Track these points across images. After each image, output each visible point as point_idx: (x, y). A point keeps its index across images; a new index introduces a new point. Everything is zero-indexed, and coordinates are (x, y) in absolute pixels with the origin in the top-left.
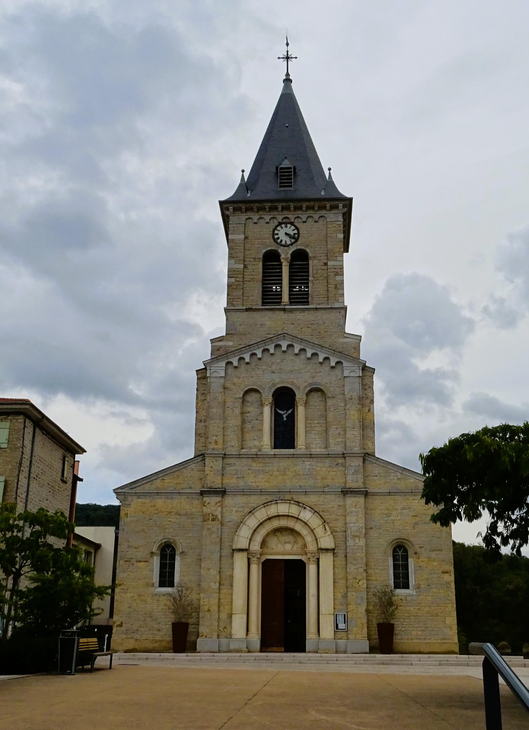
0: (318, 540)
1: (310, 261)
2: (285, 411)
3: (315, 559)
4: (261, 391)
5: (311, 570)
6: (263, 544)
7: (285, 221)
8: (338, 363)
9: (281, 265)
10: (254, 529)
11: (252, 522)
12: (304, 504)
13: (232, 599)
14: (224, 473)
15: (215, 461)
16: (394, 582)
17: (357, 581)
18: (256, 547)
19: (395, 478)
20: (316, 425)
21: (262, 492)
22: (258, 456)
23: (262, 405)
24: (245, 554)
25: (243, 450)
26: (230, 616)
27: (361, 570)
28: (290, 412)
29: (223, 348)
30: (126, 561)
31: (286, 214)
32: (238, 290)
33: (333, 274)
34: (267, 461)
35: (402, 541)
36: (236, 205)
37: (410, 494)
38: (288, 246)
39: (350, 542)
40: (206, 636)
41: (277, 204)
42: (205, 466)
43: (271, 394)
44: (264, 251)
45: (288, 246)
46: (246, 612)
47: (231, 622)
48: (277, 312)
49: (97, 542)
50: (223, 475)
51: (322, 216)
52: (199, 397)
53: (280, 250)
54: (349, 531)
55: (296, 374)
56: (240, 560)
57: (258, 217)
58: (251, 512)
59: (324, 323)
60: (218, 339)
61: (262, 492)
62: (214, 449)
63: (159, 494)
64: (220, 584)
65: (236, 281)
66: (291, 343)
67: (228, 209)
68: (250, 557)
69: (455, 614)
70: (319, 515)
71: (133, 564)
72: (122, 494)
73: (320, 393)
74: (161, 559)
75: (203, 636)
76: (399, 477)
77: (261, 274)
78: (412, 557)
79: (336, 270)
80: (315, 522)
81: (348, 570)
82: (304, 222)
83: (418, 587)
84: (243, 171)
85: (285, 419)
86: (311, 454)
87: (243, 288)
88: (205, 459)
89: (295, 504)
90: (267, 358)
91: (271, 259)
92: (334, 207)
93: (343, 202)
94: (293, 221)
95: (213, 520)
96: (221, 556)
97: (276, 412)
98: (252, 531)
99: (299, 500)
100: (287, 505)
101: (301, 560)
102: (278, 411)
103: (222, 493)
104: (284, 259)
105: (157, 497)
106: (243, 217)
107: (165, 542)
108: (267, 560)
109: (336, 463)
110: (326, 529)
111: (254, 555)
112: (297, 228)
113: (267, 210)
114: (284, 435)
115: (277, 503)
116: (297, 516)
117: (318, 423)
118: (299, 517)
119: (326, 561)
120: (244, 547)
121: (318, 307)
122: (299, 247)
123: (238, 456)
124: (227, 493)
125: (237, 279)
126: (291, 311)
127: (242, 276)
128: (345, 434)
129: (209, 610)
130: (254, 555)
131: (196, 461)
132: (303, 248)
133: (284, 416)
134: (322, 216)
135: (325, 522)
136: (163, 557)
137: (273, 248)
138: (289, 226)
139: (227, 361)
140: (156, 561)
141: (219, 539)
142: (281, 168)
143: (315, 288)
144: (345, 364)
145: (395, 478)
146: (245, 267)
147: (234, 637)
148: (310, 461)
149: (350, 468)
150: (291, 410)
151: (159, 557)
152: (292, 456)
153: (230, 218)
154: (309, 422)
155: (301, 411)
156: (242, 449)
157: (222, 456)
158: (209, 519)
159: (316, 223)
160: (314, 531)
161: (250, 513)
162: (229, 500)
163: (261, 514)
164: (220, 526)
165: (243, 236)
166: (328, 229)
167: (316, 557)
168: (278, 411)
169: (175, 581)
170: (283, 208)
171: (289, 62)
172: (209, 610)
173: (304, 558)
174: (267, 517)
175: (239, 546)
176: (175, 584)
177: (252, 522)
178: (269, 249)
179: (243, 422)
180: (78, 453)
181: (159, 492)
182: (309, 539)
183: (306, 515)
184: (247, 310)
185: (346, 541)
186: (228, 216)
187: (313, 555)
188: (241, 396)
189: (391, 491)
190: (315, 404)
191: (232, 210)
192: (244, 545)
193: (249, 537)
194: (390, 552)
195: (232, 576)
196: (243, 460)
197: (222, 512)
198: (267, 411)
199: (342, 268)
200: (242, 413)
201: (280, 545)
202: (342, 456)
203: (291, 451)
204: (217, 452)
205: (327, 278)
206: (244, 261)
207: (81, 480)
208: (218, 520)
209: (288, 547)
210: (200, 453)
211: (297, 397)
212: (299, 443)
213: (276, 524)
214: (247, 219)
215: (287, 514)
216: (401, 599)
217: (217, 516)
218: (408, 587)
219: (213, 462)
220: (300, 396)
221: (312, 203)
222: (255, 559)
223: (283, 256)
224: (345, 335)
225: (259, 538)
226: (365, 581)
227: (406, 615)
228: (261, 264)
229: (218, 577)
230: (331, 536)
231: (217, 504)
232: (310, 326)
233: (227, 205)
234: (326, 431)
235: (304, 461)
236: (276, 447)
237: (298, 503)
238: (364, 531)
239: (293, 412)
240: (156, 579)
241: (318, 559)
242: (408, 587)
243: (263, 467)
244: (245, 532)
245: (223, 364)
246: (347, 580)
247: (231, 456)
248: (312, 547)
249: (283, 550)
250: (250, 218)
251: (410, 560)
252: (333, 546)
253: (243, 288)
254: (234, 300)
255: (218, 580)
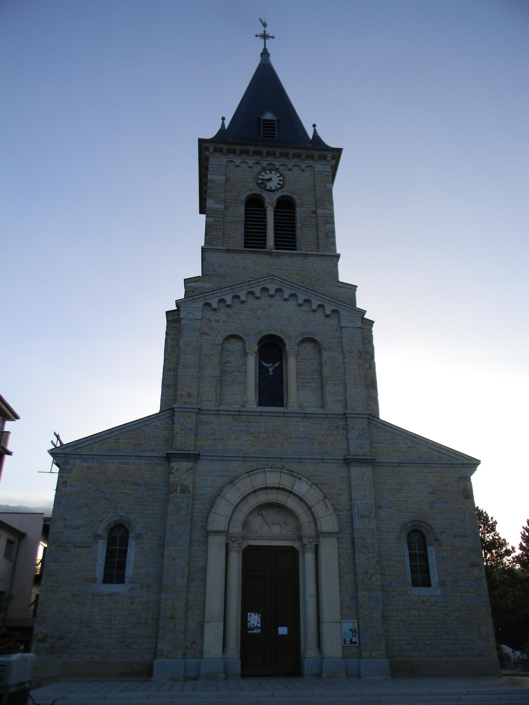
0: (318, 520)
1: (298, 209)
2: (271, 364)
3: (312, 546)
4: (245, 338)
5: (308, 560)
6: (245, 524)
7: (269, 167)
8: (335, 311)
9: (265, 211)
10: (235, 504)
11: (233, 495)
12: (298, 474)
13: (205, 601)
14: (197, 432)
15: (187, 417)
16: (412, 579)
17: (369, 576)
18: (236, 529)
19: (406, 446)
20: (310, 381)
21: (245, 459)
22: (241, 413)
23: (245, 353)
24: (222, 539)
25: (222, 406)
26: (201, 625)
27: (373, 561)
28: (277, 365)
29: (199, 290)
30: (59, 546)
31: (270, 159)
32: (218, 230)
33: (322, 222)
34: (251, 420)
35: (419, 523)
36: (217, 146)
37: (424, 465)
38: (273, 191)
39: (358, 525)
40: (167, 656)
41: (262, 149)
42: (173, 423)
43: (256, 342)
44: (247, 194)
45: (273, 191)
46: (222, 619)
47: (202, 633)
48: (263, 256)
49: (23, 530)
50: (196, 434)
51: (309, 166)
52: (169, 342)
53: (265, 195)
54: (356, 510)
55: (286, 319)
56: (216, 545)
57: (240, 161)
58: (232, 482)
59: (315, 270)
60: (193, 280)
61: (245, 459)
62: (186, 403)
63: (112, 457)
64: (189, 580)
65: (215, 221)
66: (280, 287)
67: (207, 149)
68: (229, 542)
69: (490, 621)
70: (318, 487)
71: (69, 551)
72: (63, 455)
73: (312, 345)
74: (109, 544)
75: (162, 655)
76: (409, 445)
77: (243, 216)
78: (432, 545)
79: (326, 219)
80: (312, 496)
81: (357, 560)
82: (290, 170)
83: (442, 584)
84: (223, 119)
85: (271, 373)
86: (306, 414)
87: (223, 229)
88: (174, 415)
89: (287, 473)
90: (252, 302)
91: (254, 204)
92: (323, 158)
93: (332, 153)
94: (278, 167)
95: (182, 491)
96: (191, 541)
97: (260, 364)
98: (233, 507)
99: (292, 469)
100: (278, 474)
101: (293, 547)
102: (263, 363)
103: (196, 457)
104: (269, 203)
105: (110, 461)
106: (224, 160)
107: (115, 521)
108: (249, 547)
109: (335, 425)
110: (327, 506)
111: (234, 539)
112: (281, 175)
113: (251, 153)
114: (271, 391)
115: (265, 472)
116: (290, 489)
117: (312, 379)
118: (293, 490)
119: (329, 550)
120: (222, 529)
121: (308, 253)
122: (285, 194)
123: (216, 412)
124: (201, 458)
125: (217, 219)
126: (278, 256)
127: (222, 216)
128: (346, 391)
129: (172, 617)
130: (234, 539)
131: (161, 418)
132: (290, 194)
133: (270, 370)
134: (309, 166)
135: (325, 497)
136: (111, 541)
137: (257, 192)
138: (274, 172)
139: (205, 302)
140: (102, 547)
141: (190, 517)
142: (264, 120)
143: (304, 234)
144: (342, 312)
145: (406, 446)
146: (226, 208)
147: (206, 656)
148: (304, 422)
149: (353, 431)
150: (279, 363)
151: (106, 541)
152: (282, 415)
153: (210, 159)
154: (301, 376)
155: (292, 365)
156: (220, 404)
157: (197, 410)
158: (176, 491)
159: (303, 173)
160: (313, 508)
161: (230, 483)
162: (202, 466)
163: (245, 485)
164: (191, 499)
165: (223, 178)
166: (316, 179)
167: (315, 543)
168: (263, 363)
169: (126, 575)
170: (268, 154)
171: (267, 41)
172: (172, 617)
173: (296, 545)
174: (253, 489)
175: (216, 527)
176: (127, 580)
177: (233, 495)
178: (253, 192)
179: (223, 372)
180: (9, 419)
181: (111, 454)
182: (305, 518)
183: (302, 488)
184: (228, 251)
185: (352, 523)
186: (207, 159)
187: (311, 540)
188: (221, 342)
189: (402, 461)
190: (308, 357)
191: (211, 151)
192: (222, 527)
193: (229, 516)
194: (404, 538)
195: (205, 569)
196: (222, 417)
197: (194, 483)
198: (252, 362)
199: (332, 217)
200: (221, 362)
201: (266, 528)
202: (342, 416)
203: (282, 409)
204: (190, 406)
205: (317, 226)
206: (225, 202)
207: (10, 453)
208: (189, 492)
209: (276, 529)
210: (169, 407)
211: (288, 348)
212: (290, 400)
213: (263, 498)
214: (229, 161)
215: (277, 486)
216: (423, 601)
217: (187, 487)
218: (429, 585)
219: (184, 418)
220: (290, 346)
221: (300, 151)
222: (235, 545)
223: (267, 200)
224: (339, 284)
225: (240, 517)
226: (379, 576)
227: (431, 622)
228: (243, 208)
229: (187, 569)
230: (334, 516)
231: (188, 470)
232: (298, 272)
233: (207, 145)
234: (322, 387)
235: (297, 422)
236: (260, 404)
237: (291, 473)
238: (374, 509)
239: (281, 365)
240: (100, 573)
241: (317, 546)
242: (429, 585)
243: (247, 427)
244: (223, 509)
245: (200, 305)
246: (355, 574)
247: (207, 412)
248: (308, 530)
249: (271, 533)
250: (231, 161)
251: (429, 548)
252: (336, 529)
253: (223, 229)
254: (214, 240)
255: (186, 573)
